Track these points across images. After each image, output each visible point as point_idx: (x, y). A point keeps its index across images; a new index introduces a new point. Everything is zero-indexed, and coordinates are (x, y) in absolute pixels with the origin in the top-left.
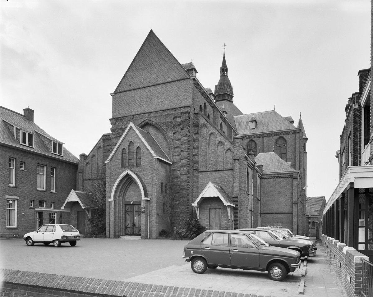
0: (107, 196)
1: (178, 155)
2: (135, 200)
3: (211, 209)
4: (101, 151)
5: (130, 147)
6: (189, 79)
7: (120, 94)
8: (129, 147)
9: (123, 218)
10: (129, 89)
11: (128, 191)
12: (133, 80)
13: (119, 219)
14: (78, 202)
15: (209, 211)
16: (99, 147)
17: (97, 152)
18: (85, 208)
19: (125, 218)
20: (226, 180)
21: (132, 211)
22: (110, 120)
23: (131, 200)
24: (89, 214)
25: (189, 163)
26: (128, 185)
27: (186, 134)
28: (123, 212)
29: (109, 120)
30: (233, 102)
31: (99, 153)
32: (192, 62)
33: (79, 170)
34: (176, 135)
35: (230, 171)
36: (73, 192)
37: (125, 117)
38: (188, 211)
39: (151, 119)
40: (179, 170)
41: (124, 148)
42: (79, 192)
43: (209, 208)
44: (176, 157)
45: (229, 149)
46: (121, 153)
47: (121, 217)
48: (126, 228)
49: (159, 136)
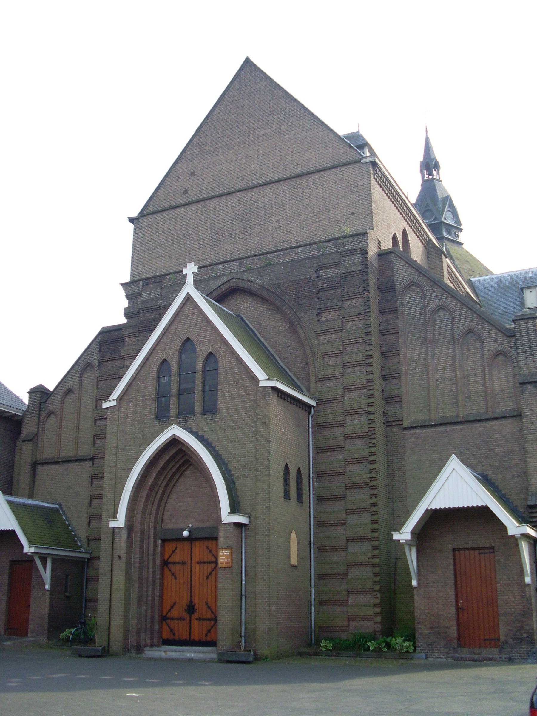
0: (104, 514)
1: (334, 378)
2: (197, 525)
3: (459, 549)
4: (90, 377)
5: (183, 357)
6: (359, 165)
7: (155, 215)
8: (180, 357)
9: (154, 584)
10: (181, 201)
11: (173, 496)
12: (195, 178)
13: (140, 587)
15: (451, 557)
17: (81, 381)
18: (33, 550)
19: (162, 584)
20: (499, 450)
21: (184, 563)
23: (182, 526)
24: (45, 570)
25: (371, 400)
26: (172, 477)
27: (359, 314)
28: (154, 563)
29: (121, 288)
30: (462, 244)
31: (85, 382)
32: (359, 131)
33: (22, 436)
34: (325, 316)
35: (509, 421)
37: (168, 274)
38: (376, 561)
39: (246, 276)
40: (341, 425)
41: (165, 361)
42: (18, 500)
43: (450, 547)
44: (329, 384)
45: (499, 353)
46: (155, 376)
47: (150, 582)
48: (164, 618)
49: (272, 323)
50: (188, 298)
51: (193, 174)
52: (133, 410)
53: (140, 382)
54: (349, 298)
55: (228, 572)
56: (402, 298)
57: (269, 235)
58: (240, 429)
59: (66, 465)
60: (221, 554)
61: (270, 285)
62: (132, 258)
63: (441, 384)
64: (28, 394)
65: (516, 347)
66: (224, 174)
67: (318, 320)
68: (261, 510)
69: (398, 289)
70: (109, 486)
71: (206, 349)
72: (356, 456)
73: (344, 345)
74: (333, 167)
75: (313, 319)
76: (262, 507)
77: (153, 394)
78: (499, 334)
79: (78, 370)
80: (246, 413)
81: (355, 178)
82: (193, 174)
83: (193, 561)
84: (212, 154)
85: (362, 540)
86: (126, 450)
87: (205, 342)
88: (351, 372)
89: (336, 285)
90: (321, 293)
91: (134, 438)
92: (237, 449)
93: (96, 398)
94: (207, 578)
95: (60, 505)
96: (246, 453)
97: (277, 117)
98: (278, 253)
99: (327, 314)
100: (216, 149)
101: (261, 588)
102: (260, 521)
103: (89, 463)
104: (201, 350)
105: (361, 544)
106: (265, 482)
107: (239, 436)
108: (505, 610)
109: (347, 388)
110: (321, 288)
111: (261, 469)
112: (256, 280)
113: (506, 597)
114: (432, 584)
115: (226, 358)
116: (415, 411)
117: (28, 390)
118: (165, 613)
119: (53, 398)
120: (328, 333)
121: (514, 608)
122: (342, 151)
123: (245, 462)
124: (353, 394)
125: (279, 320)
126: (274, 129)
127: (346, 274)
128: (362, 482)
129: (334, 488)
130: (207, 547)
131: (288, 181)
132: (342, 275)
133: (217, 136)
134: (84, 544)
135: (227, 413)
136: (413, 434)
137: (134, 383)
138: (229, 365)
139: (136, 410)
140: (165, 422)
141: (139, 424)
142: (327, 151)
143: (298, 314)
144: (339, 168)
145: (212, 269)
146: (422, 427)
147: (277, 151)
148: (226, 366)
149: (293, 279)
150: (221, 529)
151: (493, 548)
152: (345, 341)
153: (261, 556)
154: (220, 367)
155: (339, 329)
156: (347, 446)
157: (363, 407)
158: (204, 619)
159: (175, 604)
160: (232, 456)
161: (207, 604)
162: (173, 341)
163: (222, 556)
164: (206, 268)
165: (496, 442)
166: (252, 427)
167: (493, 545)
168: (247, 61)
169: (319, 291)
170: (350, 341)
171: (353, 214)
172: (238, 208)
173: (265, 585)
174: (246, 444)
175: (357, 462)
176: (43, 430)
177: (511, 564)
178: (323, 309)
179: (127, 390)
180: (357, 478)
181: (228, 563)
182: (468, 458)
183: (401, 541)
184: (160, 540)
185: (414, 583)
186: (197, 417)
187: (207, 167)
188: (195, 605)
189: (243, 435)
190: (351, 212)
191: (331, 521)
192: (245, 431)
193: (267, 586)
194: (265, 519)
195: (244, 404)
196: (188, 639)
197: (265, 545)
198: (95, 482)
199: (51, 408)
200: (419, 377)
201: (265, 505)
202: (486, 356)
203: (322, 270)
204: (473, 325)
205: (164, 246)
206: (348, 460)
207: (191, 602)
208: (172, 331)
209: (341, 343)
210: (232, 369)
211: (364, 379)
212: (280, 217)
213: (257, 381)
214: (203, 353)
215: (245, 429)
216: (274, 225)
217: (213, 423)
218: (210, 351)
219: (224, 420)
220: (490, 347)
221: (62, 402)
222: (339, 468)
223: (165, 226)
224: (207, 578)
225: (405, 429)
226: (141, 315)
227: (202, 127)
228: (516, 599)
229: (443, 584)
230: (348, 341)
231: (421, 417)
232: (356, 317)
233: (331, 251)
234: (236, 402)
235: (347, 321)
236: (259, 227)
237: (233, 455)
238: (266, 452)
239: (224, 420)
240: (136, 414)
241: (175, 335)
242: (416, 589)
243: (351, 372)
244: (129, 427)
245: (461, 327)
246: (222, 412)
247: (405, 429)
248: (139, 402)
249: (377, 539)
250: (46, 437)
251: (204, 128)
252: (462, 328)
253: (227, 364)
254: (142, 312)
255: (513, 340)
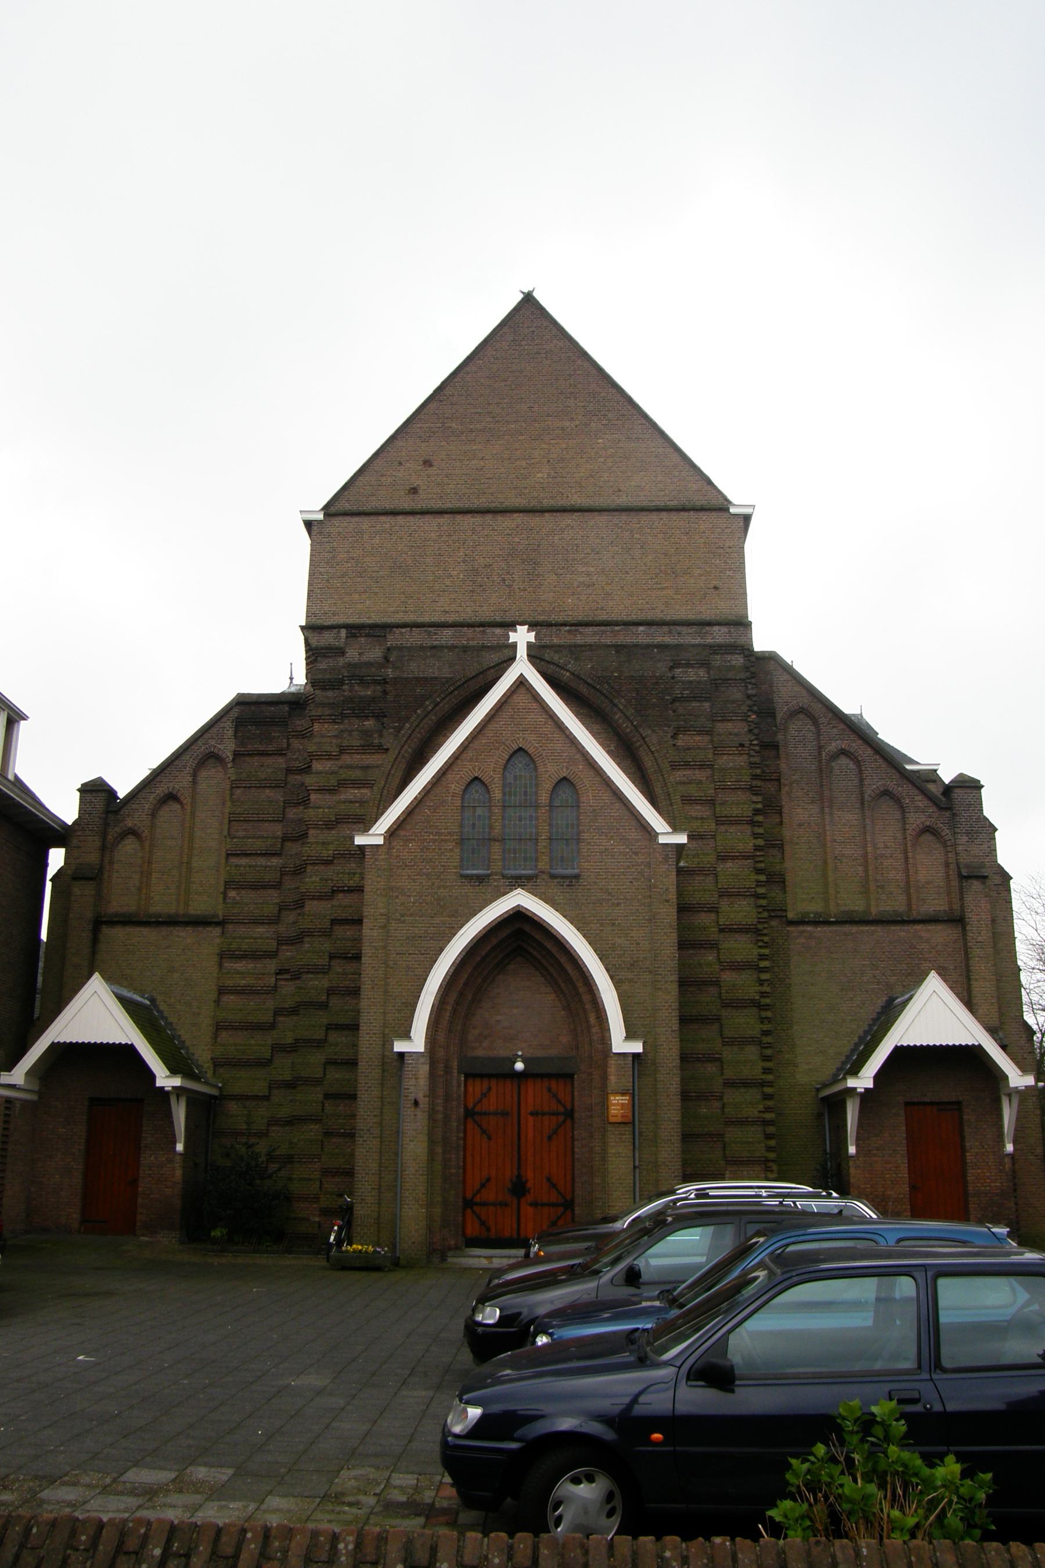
12: (431, 471)
14: (129, 1050)
16: (212, 757)
17: (194, 782)
18: (177, 1082)
22: (302, 628)
27: (742, 745)
31: (202, 786)
34: (682, 741)
35: (939, 927)
36: (96, 988)
45: (927, 830)
48: (468, 1204)
50: (522, 682)
51: (428, 463)
52: (416, 856)
53: (429, 810)
54: (725, 718)
55: (625, 1131)
56: (786, 729)
57: (573, 594)
58: (623, 905)
59: (165, 930)
60: (613, 1102)
61: (592, 675)
62: (310, 584)
63: (841, 863)
64: (78, 794)
65: (953, 824)
66: (488, 476)
67: (674, 745)
68: (663, 1034)
69: (779, 716)
70: (373, 981)
71: (555, 771)
72: (739, 958)
73: (716, 789)
74: (684, 509)
75: (666, 742)
76: (666, 1031)
77: (457, 832)
78: (926, 802)
79: (190, 761)
80: (631, 882)
81: (719, 534)
82: (428, 463)
83: (523, 1111)
84: (463, 438)
85: (746, 1084)
86: (404, 922)
87: (554, 759)
88: (727, 831)
89: (703, 695)
90: (677, 704)
91: (420, 903)
92: (618, 937)
93: (230, 817)
94: (550, 1138)
95: (153, 1000)
96: (633, 944)
97: (582, 404)
98: (602, 628)
99: (686, 737)
100: (471, 431)
101: (666, 1156)
102: (663, 1052)
103: (217, 931)
104: (547, 771)
105: (743, 1091)
106: (670, 992)
107: (621, 916)
108: (977, 1188)
109: (722, 854)
110: (680, 696)
111: (662, 971)
112: (566, 665)
113: (979, 1171)
114: (875, 1152)
115: (593, 790)
116: (802, 899)
117: (79, 786)
118: (469, 1196)
119: (134, 806)
120: (689, 767)
121: (989, 1186)
122: (695, 487)
123: (632, 958)
124: (729, 864)
125: (598, 733)
126: (577, 423)
127: (719, 681)
128: (746, 998)
129: (703, 1004)
130: (549, 1090)
131: (607, 513)
132: (713, 682)
133: (473, 411)
134: (206, 1072)
135: (597, 879)
136: (804, 931)
137: (417, 810)
138: (599, 803)
139: (421, 856)
140: (482, 882)
141: (429, 879)
142: (669, 481)
143: (641, 730)
144: (692, 512)
145: (484, 632)
146: (816, 923)
147: (584, 460)
148: (593, 803)
149: (632, 673)
150: (612, 1062)
151: (959, 1103)
152: (718, 784)
153: (665, 1106)
154: (584, 803)
155: (708, 763)
156: (721, 942)
157: (748, 886)
158: (543, 1205)
159: (489, 1180)
160: (610, 948)
161: (549, 1179)
162: (491, 749)
163: (614, 1105)
164: (471, 630)
165: (922, 954)
166: (644, 904)
167: (961, 1099)
168: (528, 300)
169: (674, 701)
170: (726, 783)
171: (716, 588)
172: (517, 540)
173: (674, 1151)
174: (633, 930)
175: (737, 967)
176: (111, 863)
177: (985, 1126)
178: (682, 729)
179: (404, 820)
180: (741, 991)
181: (626, 1116)
182: (883, 974)
183: (859, 1090)
184: (463, 1075)
185: (852, 1150)
186: (543, 879)
187: (454, 457)
188: (527, 1181)
189: (627, 916)
190: (713, 585)
191: (698, 1054)
192: (630, 910)
193: (676, 1152)
194: (670, 1049)
195: (629, 866)
196: (515, 1236)
197: (671, 1090)
198: (226, 964)
199: (129, 823)
200: (810, 849)
201: (671, 1027)
202: (909, 832)
203: (679, 668)
204: (891, 785)
205: (374, 574)
206: (725, 964)
207: (519, 1176)
208: (489, 732)
209: (712, 785)
210: (605, 809)
211: (751, 844)
212: (592, 569)
213: (653, 834)
214: (550, 776)
215: (631, 908)
216: (582, 579)
217: (573, 892)
218: (564, 775)
219: (594, 889)
220: (916, 820)
221: (153, 814)
222: (712, 974)
223: (377, 540)
224: (550, 1138)
225: (791, 923)
226: (346, 687)
227: (445, 388)
228: (993, 1174)
229: (890, 1152)
230: (723, 783)
231: (815, 909)
232: (735, 749)
233: (693, 642)
234: (614, 862)
235: (720, 752)
236: (555, 577)
237: (610, 946)
238: (670, 946)
239: (594, 889)
240: (423, 862)
241: (496, 740)
242: (853, 1159)
243: (727, 831)
244: (409, 883)
245: (874, 784)
246: (588, 876)
247: (791, 923)
248: (429, 842)
249: (770, 1084)
250: (115, 875)
251: (447, 391)
252: (875, 786)
253: (596, 800)
254: (346, 682)
255: (947, 814)
